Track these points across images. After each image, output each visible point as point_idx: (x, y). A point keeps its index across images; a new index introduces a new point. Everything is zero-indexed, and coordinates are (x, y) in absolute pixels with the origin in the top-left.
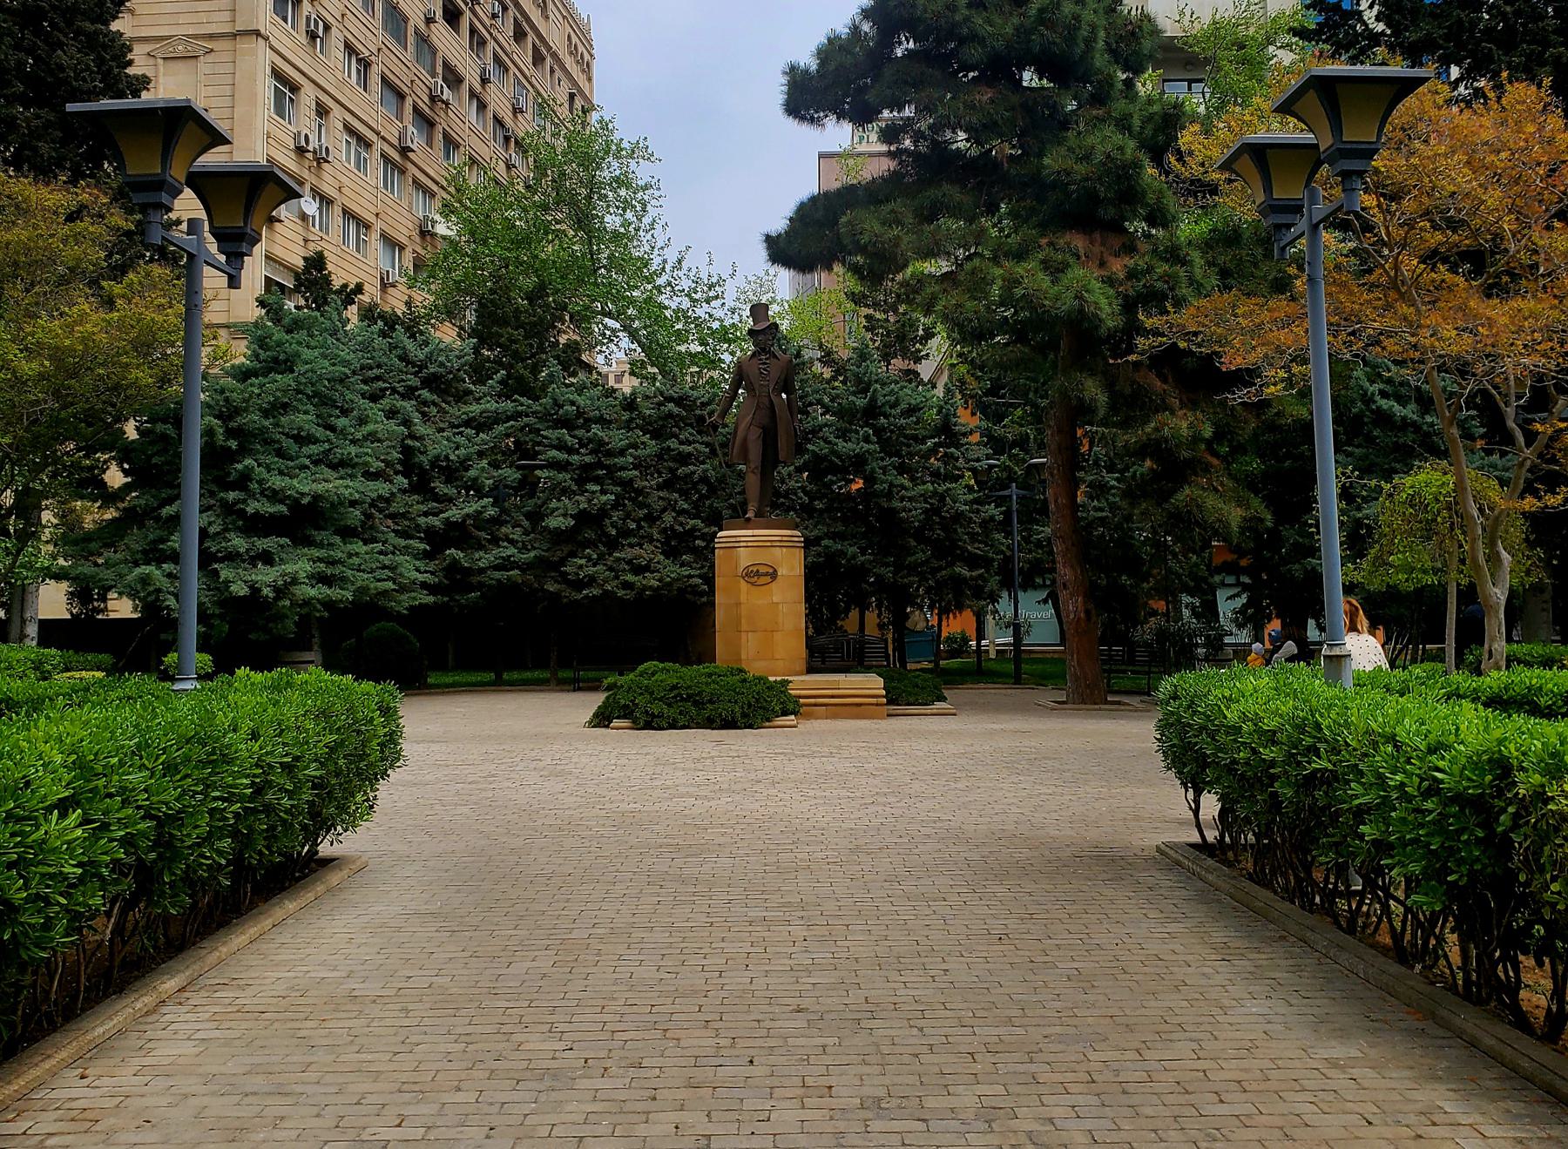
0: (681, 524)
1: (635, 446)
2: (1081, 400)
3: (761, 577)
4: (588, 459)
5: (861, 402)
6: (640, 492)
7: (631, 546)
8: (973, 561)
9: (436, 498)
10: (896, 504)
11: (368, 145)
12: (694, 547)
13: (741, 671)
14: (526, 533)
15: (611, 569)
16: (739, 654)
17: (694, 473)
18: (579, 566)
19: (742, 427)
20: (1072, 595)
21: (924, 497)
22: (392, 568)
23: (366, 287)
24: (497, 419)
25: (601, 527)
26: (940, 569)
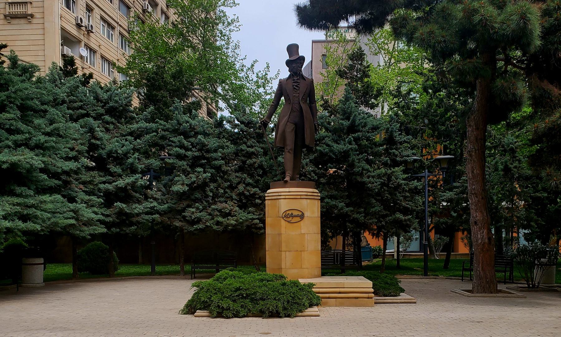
0: (248, 191)
1: (223, 148)
2: (514, 94)
3: (294, 220)
4: (196, 154)
5: (346, 123)
6: (225, 173)
8: (405, 211)
9: (111, 174)
10: (365, 179)
11: (113, 28)
12: (254, 203)
13: (282, 277)
14: (164, 195)
15: (210, 214)
16: (280, 265)
17: (255, 163)
18: (191, 212)
19: (282, 124)
20: (480, 229)
21: (379, 176)
22: (75, 212)
23: (94, 76)
24: (148, 131)
25: (205, 191)
26: (387, 216)
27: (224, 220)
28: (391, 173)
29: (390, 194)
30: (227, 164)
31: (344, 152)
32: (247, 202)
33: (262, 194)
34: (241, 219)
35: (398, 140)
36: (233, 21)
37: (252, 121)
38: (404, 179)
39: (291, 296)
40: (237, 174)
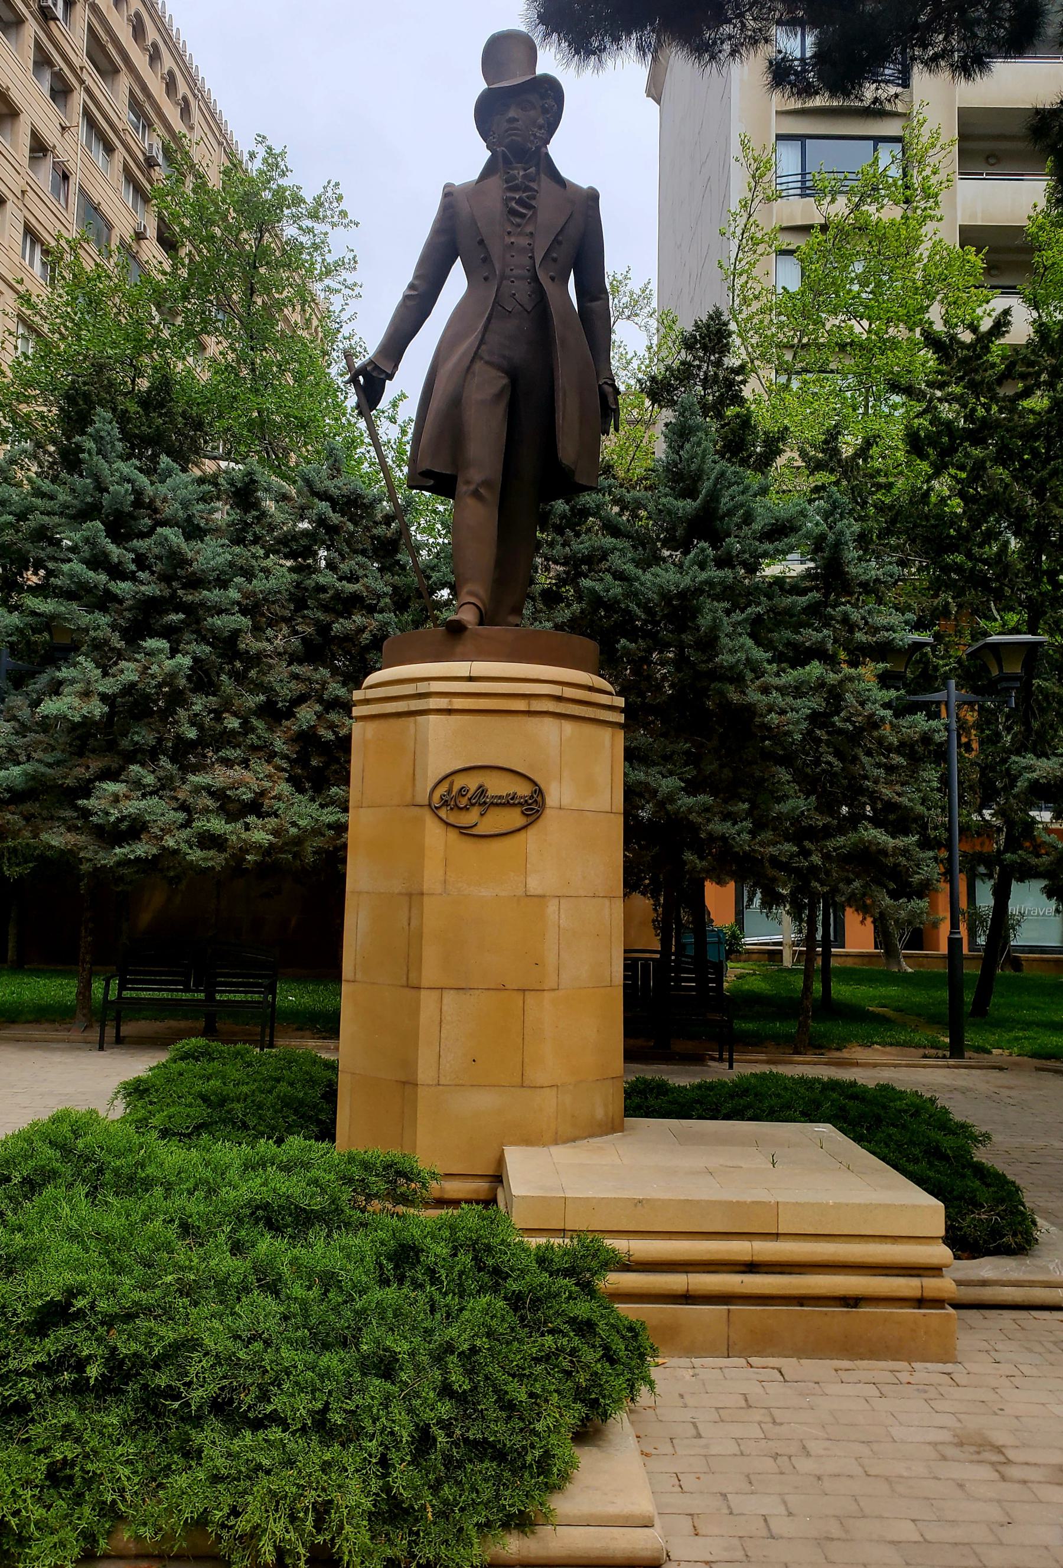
0: (332, 727)
1: (248, 574)
5: (687, 506)
6: (255, 660)
7: (228, 763)
8: (896, 819)
10: (754, 696)
15: (184, 807)
17: (361, 630)
18: (112, 800)
21: (798, 690)
27: (229, 827)
28: (841, 682)
29: (839, 754)
30: (257, 630)
31: (683, 595)
32: (327, 765)
33: (342, 692)
34: (294, 824)
35: (858, 576)
36: (340, 264)
37: (359, 496)
38: (886, 706)
39: (446, 1390)
40: (296, 668)
